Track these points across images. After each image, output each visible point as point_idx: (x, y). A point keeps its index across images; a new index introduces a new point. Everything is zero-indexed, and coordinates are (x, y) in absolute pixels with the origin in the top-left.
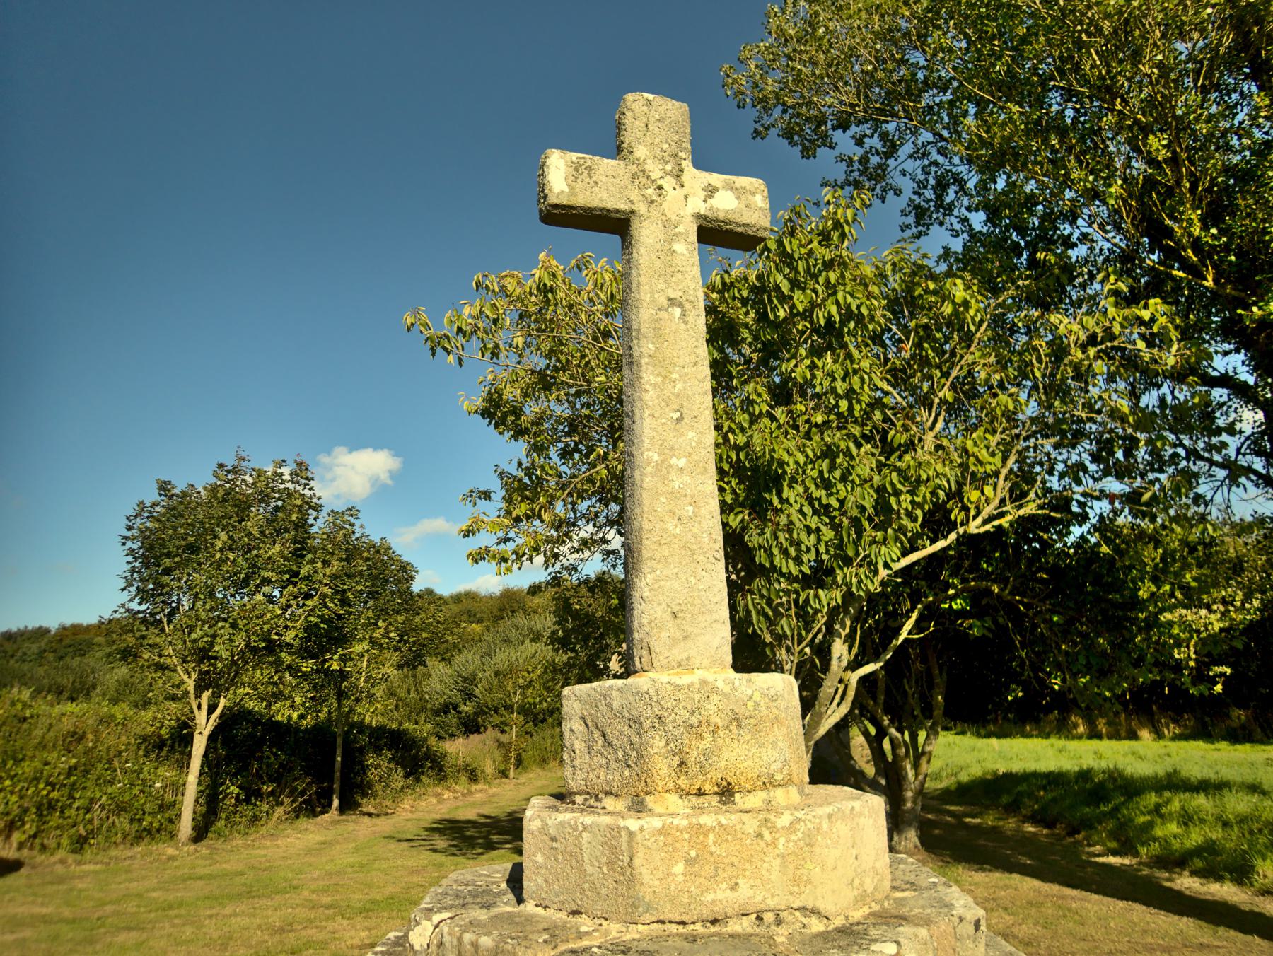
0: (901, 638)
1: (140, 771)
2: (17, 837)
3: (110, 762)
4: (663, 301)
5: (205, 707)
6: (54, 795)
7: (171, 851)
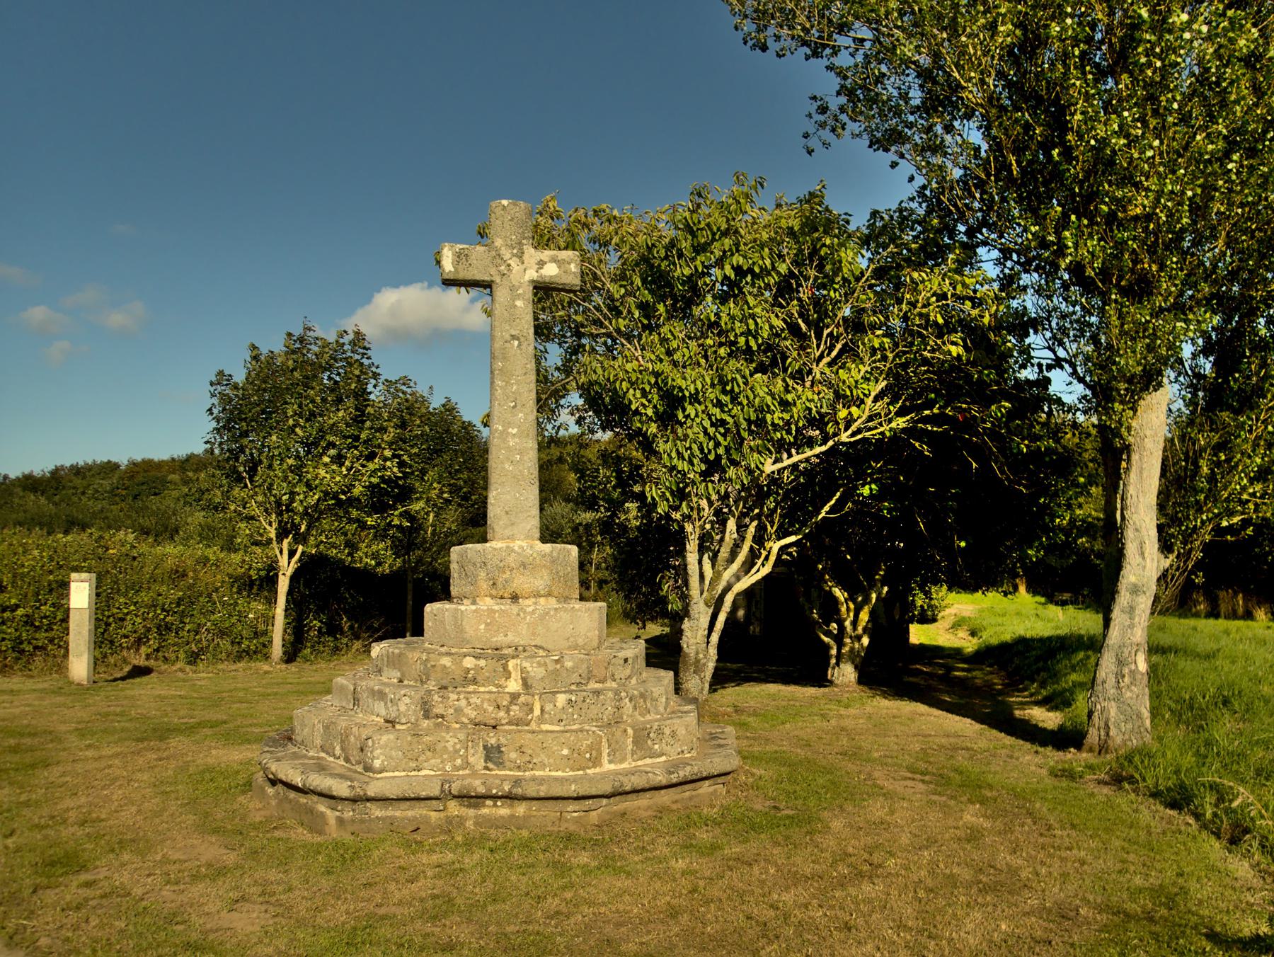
0: (823, 514)
1: (236, 604)
2: (144, 650)
3: (210, 596)
4: (508, 337)
5: (286, 552)
6: (169, 619)
7: (266, 668)
